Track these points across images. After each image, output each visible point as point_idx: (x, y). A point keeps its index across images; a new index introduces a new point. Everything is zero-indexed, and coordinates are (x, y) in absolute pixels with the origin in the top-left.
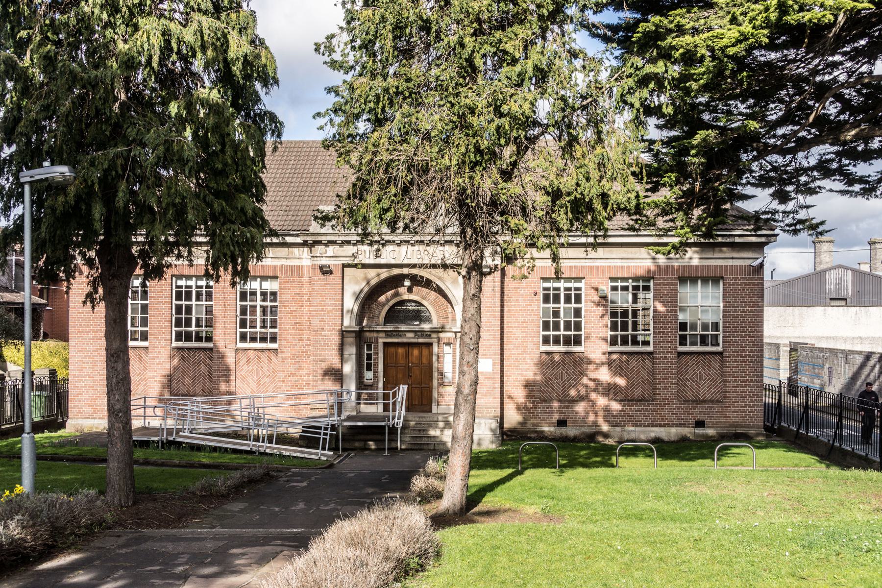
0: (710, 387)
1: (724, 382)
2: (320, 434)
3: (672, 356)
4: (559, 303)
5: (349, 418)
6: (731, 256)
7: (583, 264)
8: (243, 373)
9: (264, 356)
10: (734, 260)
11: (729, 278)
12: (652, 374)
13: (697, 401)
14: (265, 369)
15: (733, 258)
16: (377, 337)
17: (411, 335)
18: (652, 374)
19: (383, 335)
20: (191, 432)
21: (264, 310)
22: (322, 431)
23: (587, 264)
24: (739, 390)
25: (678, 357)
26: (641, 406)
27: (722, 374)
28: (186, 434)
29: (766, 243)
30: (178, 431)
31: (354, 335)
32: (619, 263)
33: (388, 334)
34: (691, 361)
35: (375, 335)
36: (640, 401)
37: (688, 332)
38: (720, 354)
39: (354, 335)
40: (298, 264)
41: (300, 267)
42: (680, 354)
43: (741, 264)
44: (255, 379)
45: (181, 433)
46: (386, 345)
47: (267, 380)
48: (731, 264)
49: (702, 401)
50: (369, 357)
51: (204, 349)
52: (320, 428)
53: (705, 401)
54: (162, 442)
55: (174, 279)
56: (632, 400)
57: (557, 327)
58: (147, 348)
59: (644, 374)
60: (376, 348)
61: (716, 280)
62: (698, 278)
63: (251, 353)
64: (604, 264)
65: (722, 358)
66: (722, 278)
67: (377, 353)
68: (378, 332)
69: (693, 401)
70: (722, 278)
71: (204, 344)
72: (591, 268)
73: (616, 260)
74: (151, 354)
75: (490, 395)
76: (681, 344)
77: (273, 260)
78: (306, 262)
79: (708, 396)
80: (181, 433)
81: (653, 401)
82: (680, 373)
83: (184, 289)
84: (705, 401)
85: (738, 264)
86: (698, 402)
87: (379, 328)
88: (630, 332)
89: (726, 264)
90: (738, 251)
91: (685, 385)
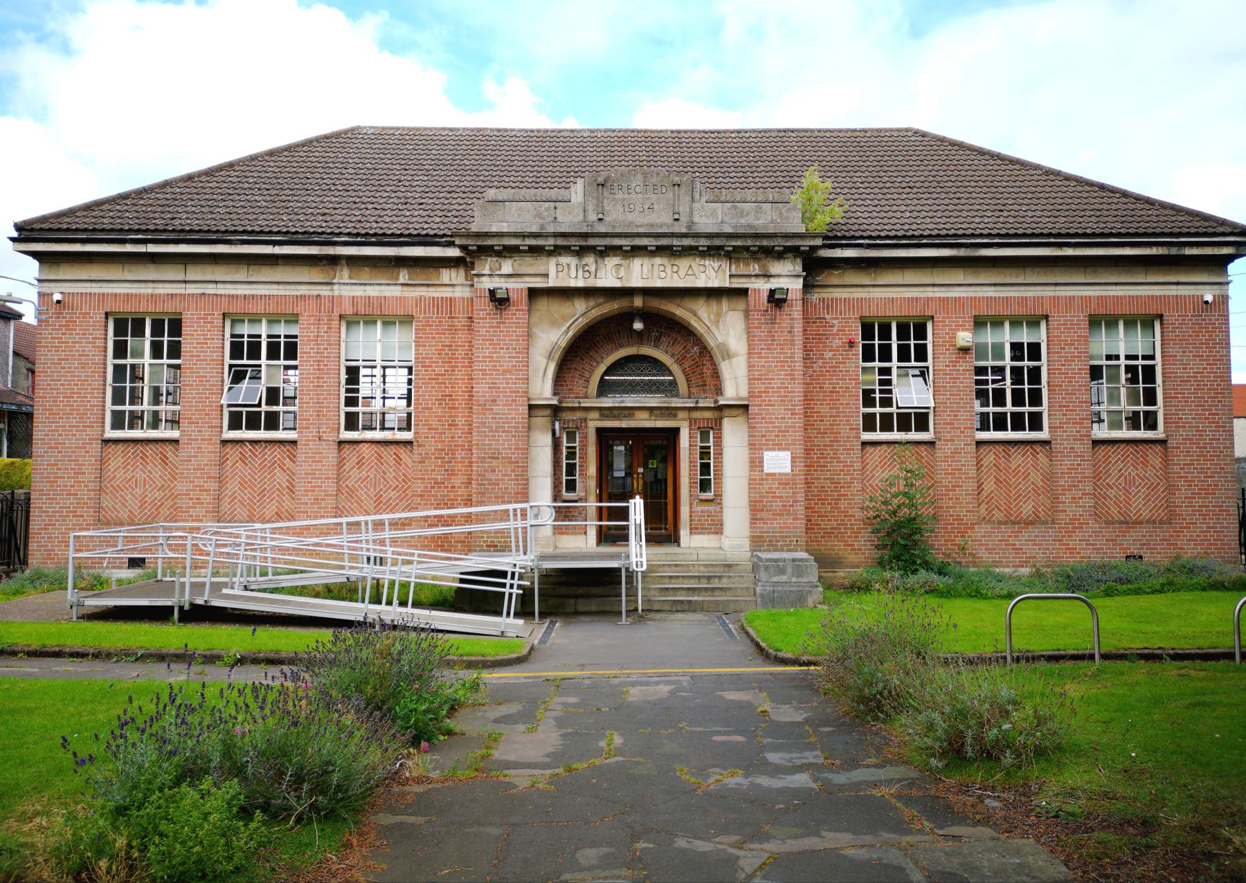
0: (1147, 499)
1: (1171, 489)
2: (504, 585)
3: (1083, 448)
4: (890, 360)
5: (544, 557)
6: (1115, 281)
7: (930, 295)
8: (350, 483)
9: (388, 453)
10: (1180, 287)
11: (1171, 316)
12: (1050, 478)
13: (1127, 523)
14: (390, 475)
15: (1178, 284)
16: (585, 420)
17: (645, 415)
18: (1050, 478)
19: (596, 415)
20: (246, 588)
21: (1017, 372)
22: (508, 581)
23: (938, 295)
24: (1197, 502)
25: (1093, 448)
26: (1033, 532)
27: (1167, 476)
28: (238, 591)
29: (1230, 258)
30: (216, 587)
31: (548, 412)
32: (990, 292)
33: (605, 412)
34: (1115, 454)
35: (579, 415)
36: (1032, 523)
37: (360, 409)
38: (1163, 442)
39: (548, 412)
40: (449, 295)
41: (451, 300)
42: (979, 443)
43: (1192, 293)
44: (372, 492)
45: (225, 591)
46: (600, 431)
47: (393, 494)
48: (1174, 293)
49: (1135, 523)
50: (571, 455)
51: (282, 442)
52: (503, 574)
53: (1141, 523)
54: (181, 608)
55: (228, 324)
56: (1019, 523)
57: (999, 398)
58: (176, 441)
59: (1036, 477)
60: (585, 438)
61: (407, 320)
62: (1005, 317)
63: (364, 447)
64: (965, 295)
65: (1166, 449)
66: (1046, 317)
67: (584, 447)
68: (587, 409)
69: (1121, 523)
70: (1046, 317)
71: (164, 433)
72: (944, 301)
73: (985, 288)
74: (943, 449)
75: (788, 514)
76: (348, 428)
77: (405, 288)
78: (461, 293)
79: (1145, 514)
80: (225, 591)
81: (1053, 522)
82: (1097, 476)
83: (246, 339)
84: (1141, 523)
85: (1187, 293)
86: (1128, 523)
87: (586, 403)
88: (1009, 408)
89: (1167, 293)
90: (1186, 272)
91: (1105, 496)
